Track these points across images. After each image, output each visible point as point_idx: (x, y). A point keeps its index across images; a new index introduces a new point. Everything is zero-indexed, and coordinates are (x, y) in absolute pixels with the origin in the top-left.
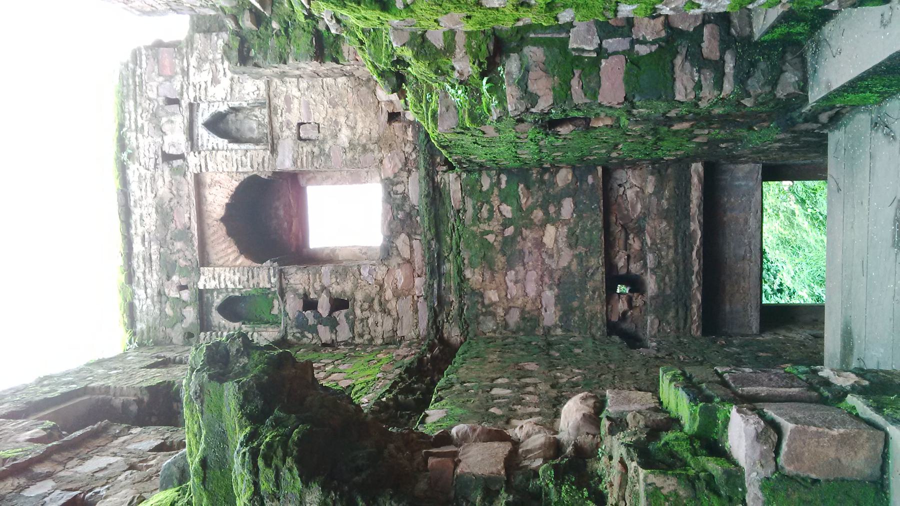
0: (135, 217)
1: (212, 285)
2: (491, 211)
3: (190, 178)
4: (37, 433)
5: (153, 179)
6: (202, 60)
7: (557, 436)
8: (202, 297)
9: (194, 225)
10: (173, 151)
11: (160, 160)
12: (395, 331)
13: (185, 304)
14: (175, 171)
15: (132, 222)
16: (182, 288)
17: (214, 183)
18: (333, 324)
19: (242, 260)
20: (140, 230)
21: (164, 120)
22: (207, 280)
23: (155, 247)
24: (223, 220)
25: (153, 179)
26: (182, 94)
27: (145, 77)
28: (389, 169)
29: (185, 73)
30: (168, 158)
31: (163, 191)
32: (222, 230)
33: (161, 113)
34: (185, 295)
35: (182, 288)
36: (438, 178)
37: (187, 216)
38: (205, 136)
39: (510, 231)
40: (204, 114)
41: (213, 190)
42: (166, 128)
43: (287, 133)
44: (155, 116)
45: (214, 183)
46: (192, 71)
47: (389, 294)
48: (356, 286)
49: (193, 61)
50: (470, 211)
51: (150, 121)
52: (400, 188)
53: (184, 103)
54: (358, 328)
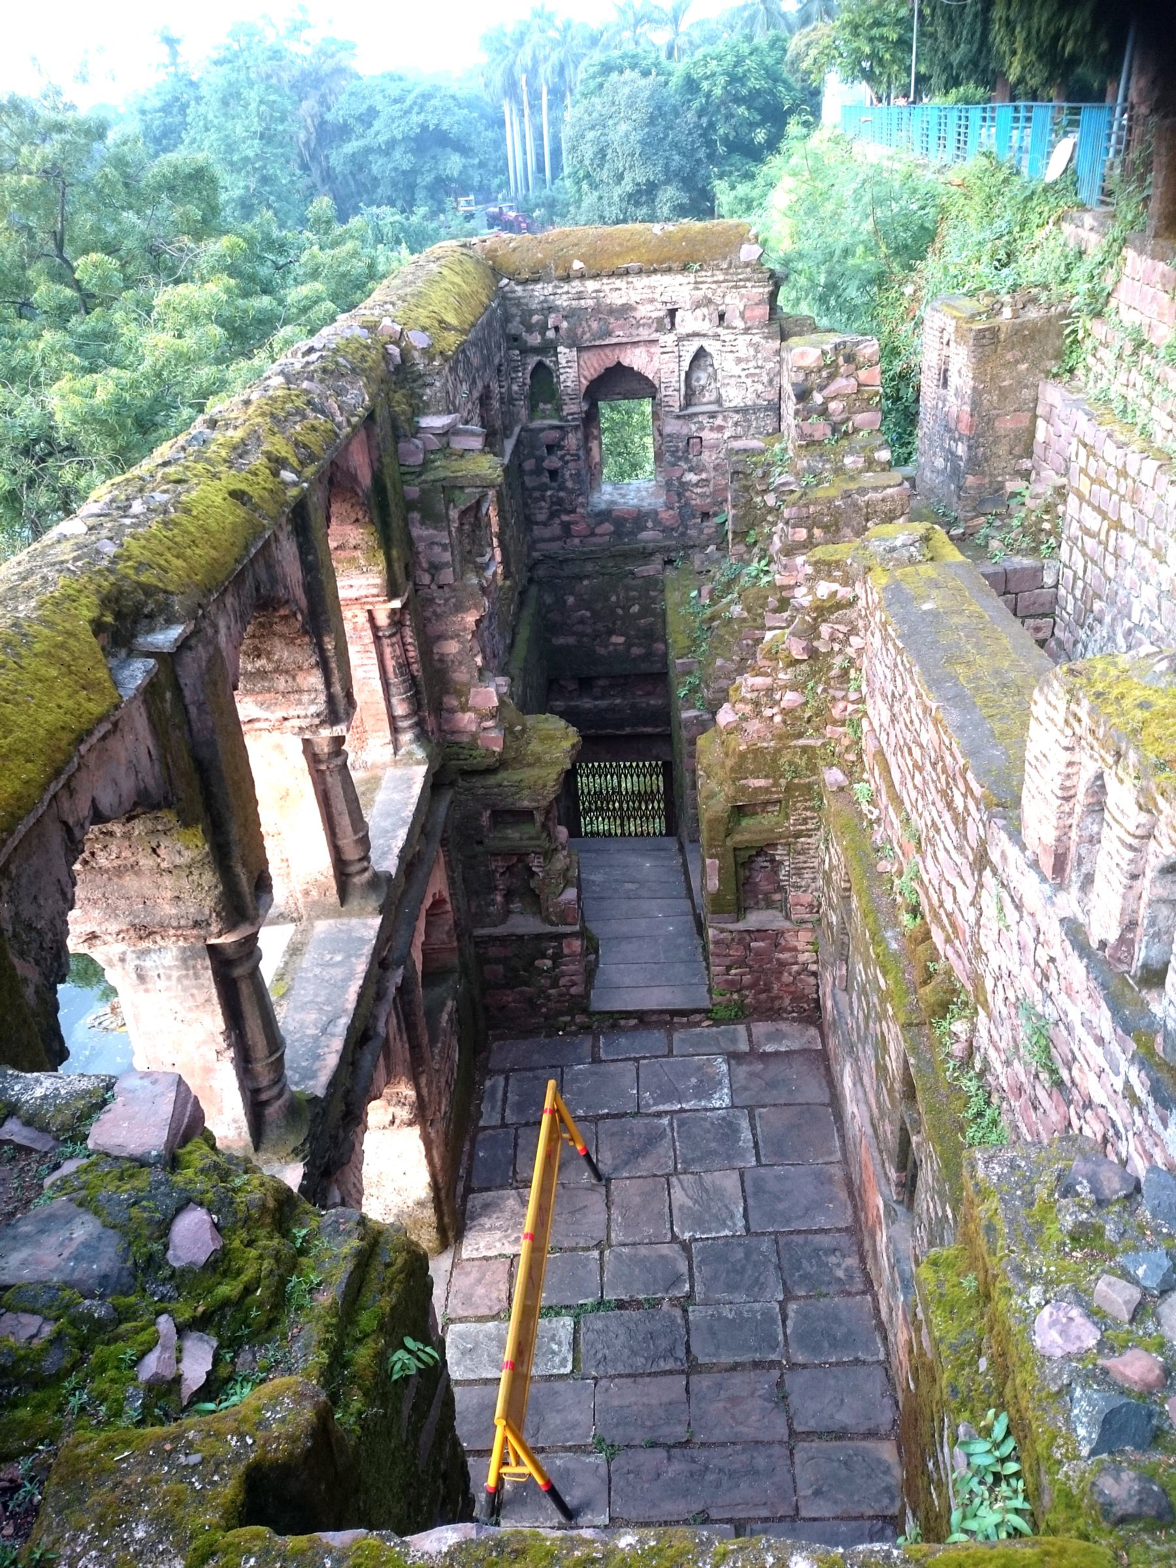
0: (618, 283)
1: (562, 360)
2: (634, 598)
3: (655, 336)
4: (858, 1080)
5: (652, 301)
6: (757, 347)
7: (1085, 322)
8: (549, 348)
9: (614, 340)
10: (678, 320)
11: (670, 307)
12: (537, 523)
13: (543, 334)
14: (660, 321)
15: (613, 280)
16: (557, 329)
17: (651, 356)
18: (538, 471)
19: (585, 383)
20: (606, 288)
21: (705, 310)
22: (565, 354)
23: (591, 303)
24: (619, 363)
25: (652, 301)
26: (728, 327)
27: (743, 291)
28: (665, 515)
29: (747, 330)
30: (672, 313)
31: (643, 311)
32: (610, 363)
33: (712, 307)
34: (551, 334)
35: (557, 329)
36: (658, 555)
37: (619, 335)
38: (691, 348)
39: (620, 611)
40: (711, 346)
41: (644, 355)
42: (699, 312)
43: (694, 428)
44: (709, 302)
45: (651, 356)
46: (748, 337)
47: (565, 518)
48: (571, 491)
49: (756, 339)
50: (634, 582)
51: (705, 297)
52: (650, 524)
53: (720, 330)
54: (537, 494)
